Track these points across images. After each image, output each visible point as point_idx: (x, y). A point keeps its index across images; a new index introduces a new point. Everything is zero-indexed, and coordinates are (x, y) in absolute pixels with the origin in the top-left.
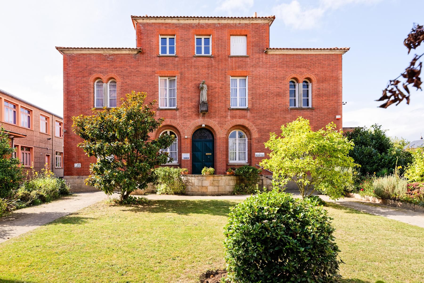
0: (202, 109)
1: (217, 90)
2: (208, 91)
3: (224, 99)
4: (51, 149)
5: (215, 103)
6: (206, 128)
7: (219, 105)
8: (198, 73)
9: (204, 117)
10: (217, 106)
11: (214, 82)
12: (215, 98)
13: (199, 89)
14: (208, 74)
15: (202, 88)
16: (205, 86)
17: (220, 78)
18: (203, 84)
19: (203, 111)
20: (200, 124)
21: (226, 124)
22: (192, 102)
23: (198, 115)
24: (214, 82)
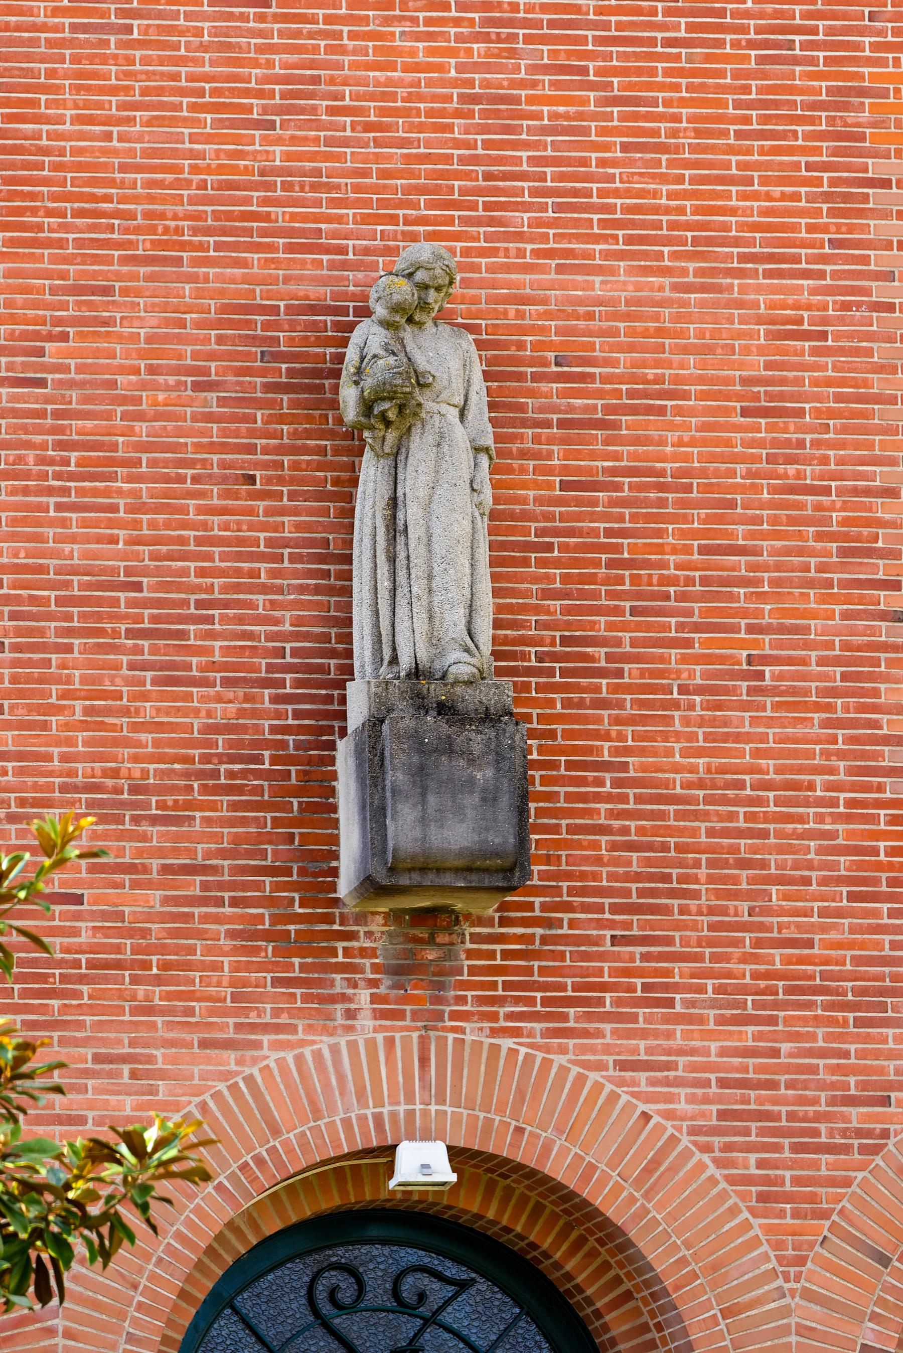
0: (404, 830)
1: (675, 442)
2: (501, 456)
3: (826, 624)
4: (459, 400)
5: (655, 704)
6: (488, 1210)
7: (722, 739)
8: (300, 90)
9: (439, 977)
10: (680, 761)
11: (622, 284)
12: (649, 604)
13: (329, 418)
14: (501, 109)
15: (397, 407)
16: (449, 359)
17: (742, 209)
18: (407, 316)
19: (426, 865)
20: (340, 1128)
21: (874, 1142)
22: (172, 677)
23: (303, 926)
24: (622, 284)
